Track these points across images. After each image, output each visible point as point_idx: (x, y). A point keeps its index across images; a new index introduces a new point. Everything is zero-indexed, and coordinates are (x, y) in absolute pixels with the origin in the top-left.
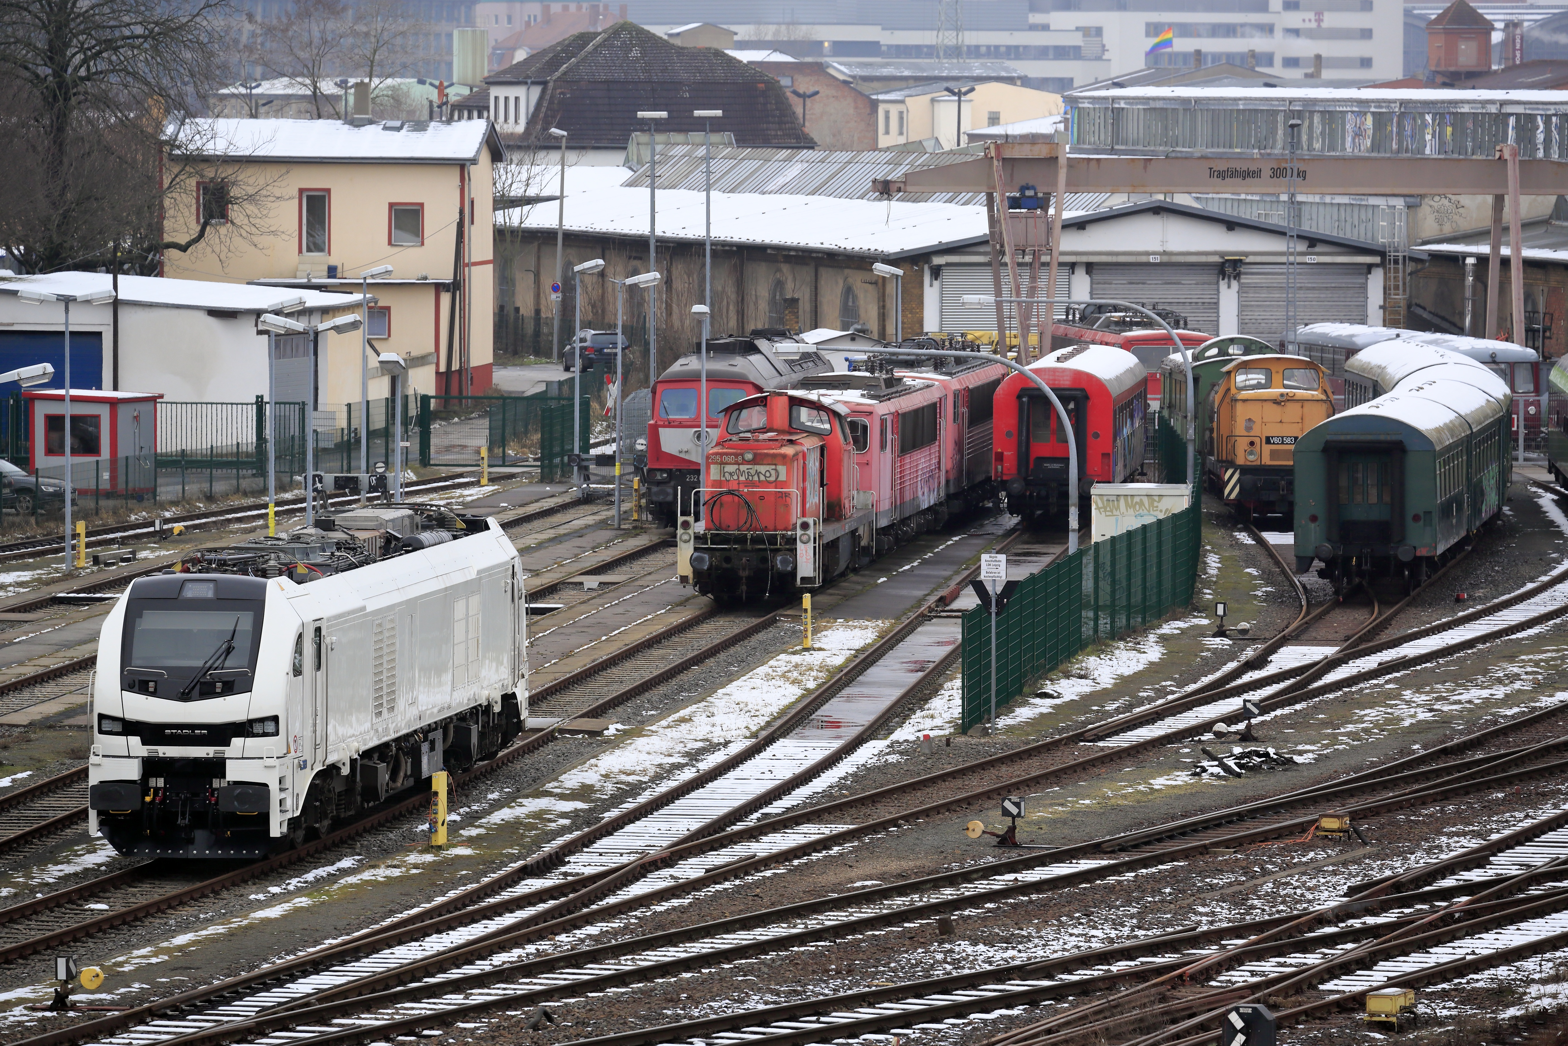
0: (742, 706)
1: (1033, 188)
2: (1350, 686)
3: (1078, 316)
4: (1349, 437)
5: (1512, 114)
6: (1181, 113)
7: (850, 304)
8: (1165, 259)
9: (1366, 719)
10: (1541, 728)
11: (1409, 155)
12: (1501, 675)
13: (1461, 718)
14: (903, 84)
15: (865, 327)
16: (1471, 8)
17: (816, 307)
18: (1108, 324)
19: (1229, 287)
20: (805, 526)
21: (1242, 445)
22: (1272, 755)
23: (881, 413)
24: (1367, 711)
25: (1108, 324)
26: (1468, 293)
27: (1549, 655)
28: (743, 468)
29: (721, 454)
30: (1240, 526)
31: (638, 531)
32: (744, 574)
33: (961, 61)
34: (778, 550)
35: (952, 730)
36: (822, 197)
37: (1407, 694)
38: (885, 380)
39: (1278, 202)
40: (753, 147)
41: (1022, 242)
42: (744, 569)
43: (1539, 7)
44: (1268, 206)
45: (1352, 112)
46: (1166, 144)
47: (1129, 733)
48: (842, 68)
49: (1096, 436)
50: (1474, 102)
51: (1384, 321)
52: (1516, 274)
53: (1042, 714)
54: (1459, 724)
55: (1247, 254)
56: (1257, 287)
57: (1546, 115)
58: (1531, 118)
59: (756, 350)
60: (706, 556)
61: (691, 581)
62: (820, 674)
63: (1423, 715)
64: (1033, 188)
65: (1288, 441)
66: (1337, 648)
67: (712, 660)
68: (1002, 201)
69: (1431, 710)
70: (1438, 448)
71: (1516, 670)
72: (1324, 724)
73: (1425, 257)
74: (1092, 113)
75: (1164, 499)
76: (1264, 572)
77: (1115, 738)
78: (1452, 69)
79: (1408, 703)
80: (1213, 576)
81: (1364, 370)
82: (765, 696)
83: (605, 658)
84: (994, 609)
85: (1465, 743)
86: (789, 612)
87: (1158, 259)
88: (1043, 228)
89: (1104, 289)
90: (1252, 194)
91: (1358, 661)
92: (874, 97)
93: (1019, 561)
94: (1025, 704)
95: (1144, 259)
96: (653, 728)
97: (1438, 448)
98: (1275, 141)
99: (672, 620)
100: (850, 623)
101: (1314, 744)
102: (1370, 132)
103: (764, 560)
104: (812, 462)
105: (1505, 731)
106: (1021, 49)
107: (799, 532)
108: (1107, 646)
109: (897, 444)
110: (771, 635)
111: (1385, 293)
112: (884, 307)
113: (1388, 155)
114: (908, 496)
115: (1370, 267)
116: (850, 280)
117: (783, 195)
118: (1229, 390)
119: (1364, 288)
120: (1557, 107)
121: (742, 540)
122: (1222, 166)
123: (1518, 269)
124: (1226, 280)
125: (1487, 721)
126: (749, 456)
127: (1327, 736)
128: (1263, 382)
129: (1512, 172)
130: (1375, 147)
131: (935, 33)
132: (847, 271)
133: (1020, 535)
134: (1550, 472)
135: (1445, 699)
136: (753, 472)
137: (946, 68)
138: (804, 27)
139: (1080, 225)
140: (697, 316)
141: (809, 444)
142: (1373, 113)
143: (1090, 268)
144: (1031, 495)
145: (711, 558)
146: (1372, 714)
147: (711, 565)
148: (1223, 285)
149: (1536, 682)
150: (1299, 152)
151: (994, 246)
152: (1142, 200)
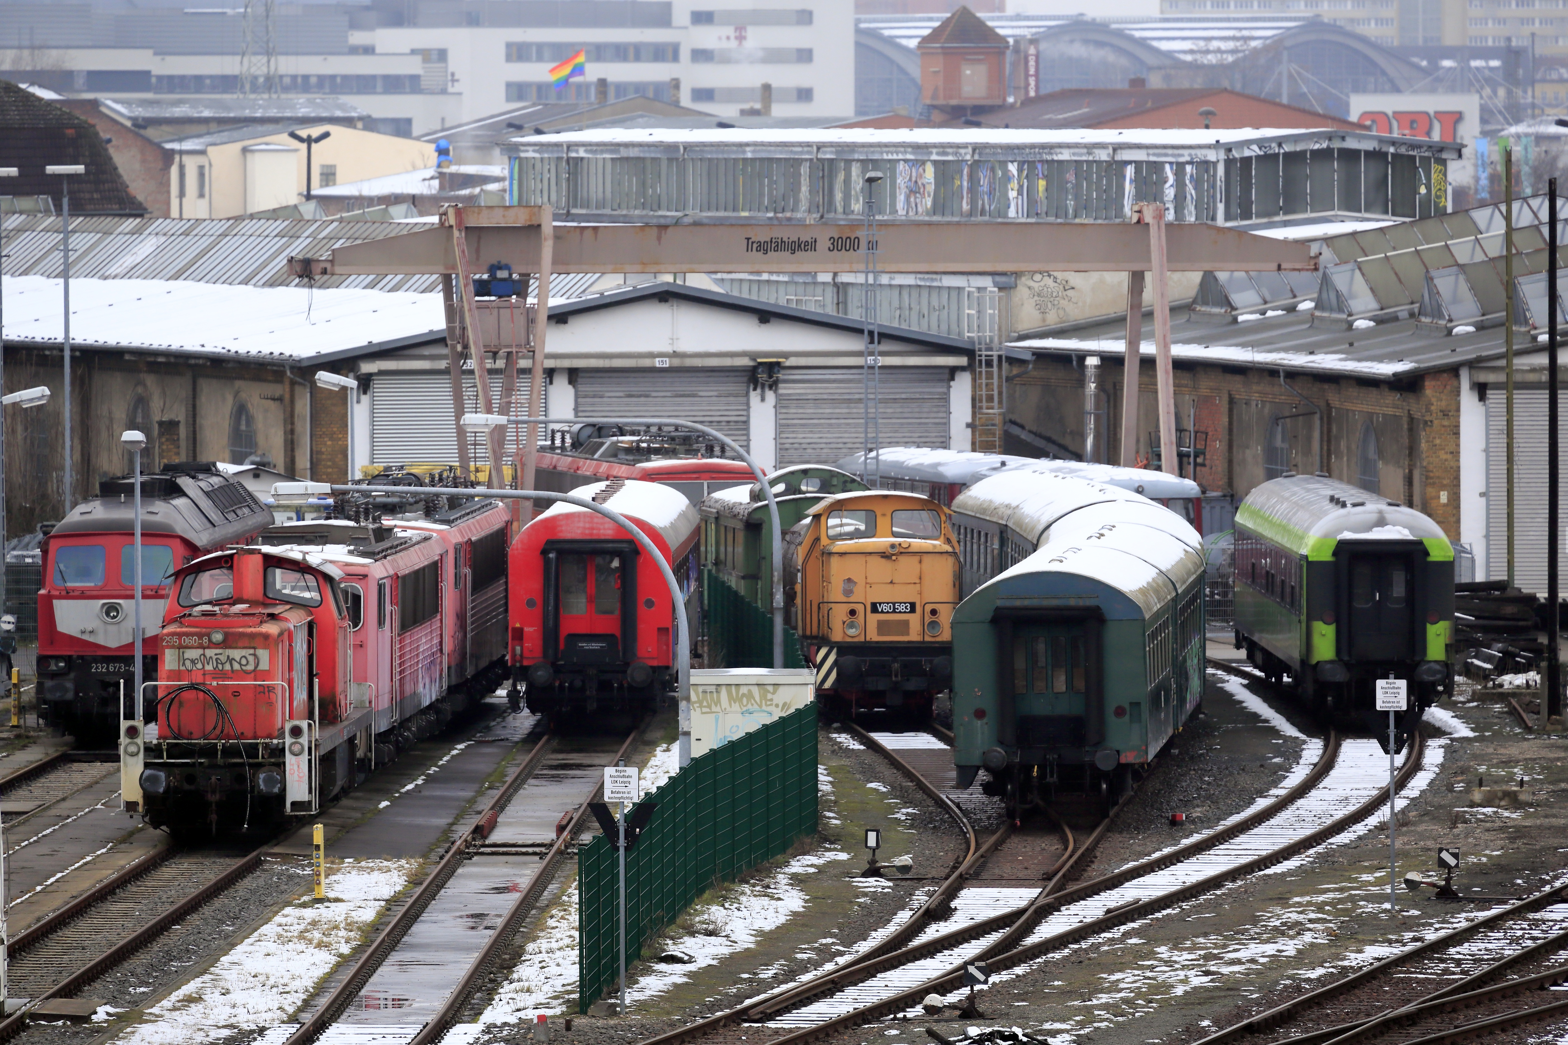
0: (262, 978)
1: (507, 267)
2: (1076, 941)
3: (568, 440)
4: (1026, 603)
5: (1130, 162)
6: (664, 165)
7: (243, 427)
8: (676, 362)
9: (1122, 985)
10: (1363, 994)
11: (986, 218)
12: (1278, 923)
13: (1251, 983)
14: (202, 128)
15: (265, 460)
16: (978, 19)
17: (194, 432)
18: (615, 453)
19: (763, 400)
20: (296, 732)
21: (839, 614)
22: (1021, 1037)
23: (378, 576)
24: (1118, 976)
25: (615, 453)
26: (1090, 405)
27: (1331, 895)
28: (210, 653)
29: (180, 635)
30: (835, 725)
31: (22, 742)
32: (214, 798)
33: (274, 96)
34: (260, 766)
35: (564, 1008)
36: (189, 283)
37: (1163, 951)
38: (374, 530)
39: (815, 283)
40: (86, 216)
41: (495, 342)
42: (214, 792)
43: (1028, 18)
44: (801, 289)
45: (906, 161)
46: (644, 206)
47: (804, 1010)
48: (118, 107)
49: (650, 603)
50: (1076, 146)
51: (973, 444)
52: (1164, 378)
53: (675, 985)
54: (1252, 993)
55: (787, 355)
56: (800, 400)
57: (1178, 164)
58: (1156, 167)
59: (179, 492)
60: (162, 775)
61: (140, 809)
62: (352, 934)
63: (1198, 981)
64: (507, 267)
65: (901, 608)
66: (1035, 892)
67: (195, 916)
68: (466, 286)
69: (1207, 973)
70: (1147, 617)
71: (1294, 917)
72: (1066, 994)
73: (1028, 357)
74: (538, 165)
75: (781, 688)
76: (893, 788)
77: (787, 1016)
78: (954, 102)
79: (1169, 963)
80: (828, 794)
81: (984, 511)
82: (290, 965)
83: (51, 915)
84: (622, 842)
85: (1273, 1017)
86: (276, 850)
87: (666, 363)
88: (521, 321)
89: (593, 404)
90: (778, 273)
91: (1072, 907)
92: (168, 146)
93: (558, 776)
94: (648, 971)
95: (646, 363)
96: (155, 1010)
97: (1147, 617)
98: (797, 201)
99: (122, 863)
100: (363, 864)
101: (1063, 1020)
102: (931, 188)
103: (241, 779)
104: (299, 644)
105: (1316, 1001)
106: (339, 80)
107: (288, 740)
108: (729, 890)
109: (396, 618)
110: (261, 882)
111: (974, 406)
112: (292, 432)
113: (956, 219)
114: (408, 689)
115: (953, 371)
116: (243, 395)
117: (133, 281)
118: (818, 539)
119: (945, 399)
120: (1193, 152)
121: (209, 751)
122: (763, 236)
123: (1167, 372)
124: (759, 391)
125: (1285, 985)
126: (218, 637)
127: (1078, 1010)
128: (862, 527)
129: (1157, 240)
130: (939, 207)
131: (238, 58)
132: (238, 383)
133: (548, 741)
134: (1238, 647)
135: (1216, 957)
136: (223, 658)
137: (260, 107)
138: (54, 52)
139: (560, 317)
140: (128, 446)
141: (296, 620)
142: (935, 163)
143: (573, 375)
144: (561, 686)
145: (167, 777)
146: (1128, 978)
147: (168, 788)
148: (754, 397)
149: (1329, 932)
150: (832, 215)
151: (454, 347)
152: (644, 282)
